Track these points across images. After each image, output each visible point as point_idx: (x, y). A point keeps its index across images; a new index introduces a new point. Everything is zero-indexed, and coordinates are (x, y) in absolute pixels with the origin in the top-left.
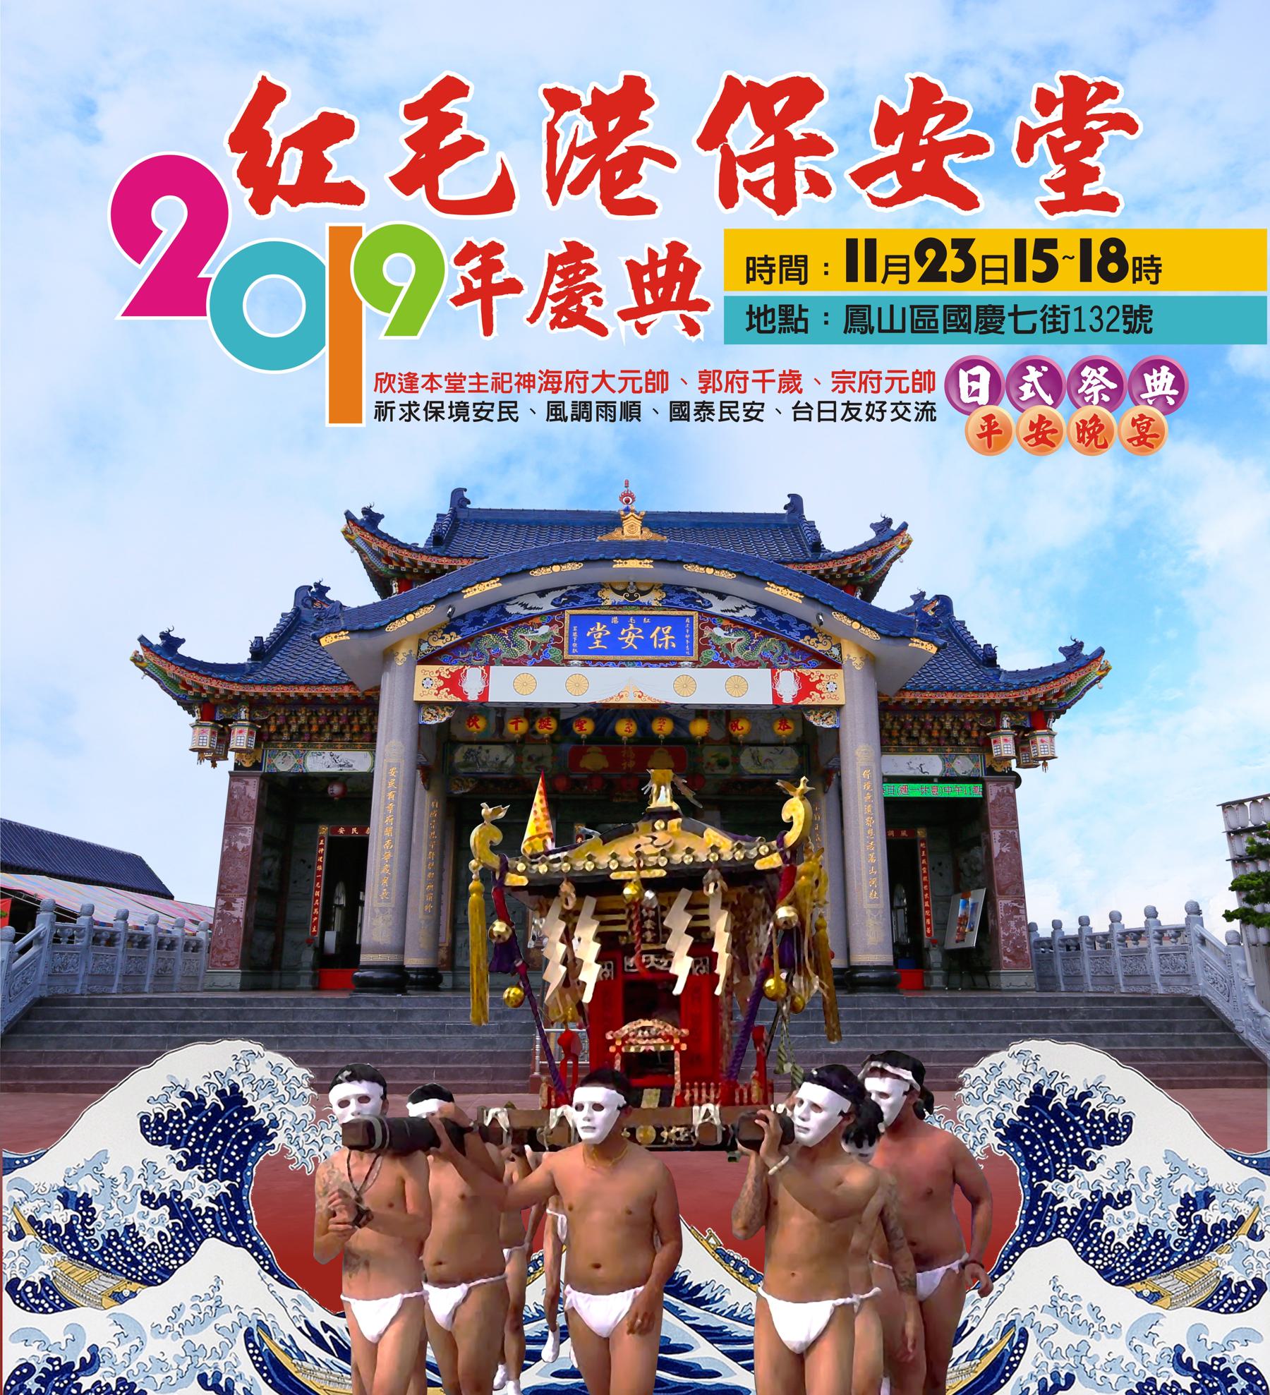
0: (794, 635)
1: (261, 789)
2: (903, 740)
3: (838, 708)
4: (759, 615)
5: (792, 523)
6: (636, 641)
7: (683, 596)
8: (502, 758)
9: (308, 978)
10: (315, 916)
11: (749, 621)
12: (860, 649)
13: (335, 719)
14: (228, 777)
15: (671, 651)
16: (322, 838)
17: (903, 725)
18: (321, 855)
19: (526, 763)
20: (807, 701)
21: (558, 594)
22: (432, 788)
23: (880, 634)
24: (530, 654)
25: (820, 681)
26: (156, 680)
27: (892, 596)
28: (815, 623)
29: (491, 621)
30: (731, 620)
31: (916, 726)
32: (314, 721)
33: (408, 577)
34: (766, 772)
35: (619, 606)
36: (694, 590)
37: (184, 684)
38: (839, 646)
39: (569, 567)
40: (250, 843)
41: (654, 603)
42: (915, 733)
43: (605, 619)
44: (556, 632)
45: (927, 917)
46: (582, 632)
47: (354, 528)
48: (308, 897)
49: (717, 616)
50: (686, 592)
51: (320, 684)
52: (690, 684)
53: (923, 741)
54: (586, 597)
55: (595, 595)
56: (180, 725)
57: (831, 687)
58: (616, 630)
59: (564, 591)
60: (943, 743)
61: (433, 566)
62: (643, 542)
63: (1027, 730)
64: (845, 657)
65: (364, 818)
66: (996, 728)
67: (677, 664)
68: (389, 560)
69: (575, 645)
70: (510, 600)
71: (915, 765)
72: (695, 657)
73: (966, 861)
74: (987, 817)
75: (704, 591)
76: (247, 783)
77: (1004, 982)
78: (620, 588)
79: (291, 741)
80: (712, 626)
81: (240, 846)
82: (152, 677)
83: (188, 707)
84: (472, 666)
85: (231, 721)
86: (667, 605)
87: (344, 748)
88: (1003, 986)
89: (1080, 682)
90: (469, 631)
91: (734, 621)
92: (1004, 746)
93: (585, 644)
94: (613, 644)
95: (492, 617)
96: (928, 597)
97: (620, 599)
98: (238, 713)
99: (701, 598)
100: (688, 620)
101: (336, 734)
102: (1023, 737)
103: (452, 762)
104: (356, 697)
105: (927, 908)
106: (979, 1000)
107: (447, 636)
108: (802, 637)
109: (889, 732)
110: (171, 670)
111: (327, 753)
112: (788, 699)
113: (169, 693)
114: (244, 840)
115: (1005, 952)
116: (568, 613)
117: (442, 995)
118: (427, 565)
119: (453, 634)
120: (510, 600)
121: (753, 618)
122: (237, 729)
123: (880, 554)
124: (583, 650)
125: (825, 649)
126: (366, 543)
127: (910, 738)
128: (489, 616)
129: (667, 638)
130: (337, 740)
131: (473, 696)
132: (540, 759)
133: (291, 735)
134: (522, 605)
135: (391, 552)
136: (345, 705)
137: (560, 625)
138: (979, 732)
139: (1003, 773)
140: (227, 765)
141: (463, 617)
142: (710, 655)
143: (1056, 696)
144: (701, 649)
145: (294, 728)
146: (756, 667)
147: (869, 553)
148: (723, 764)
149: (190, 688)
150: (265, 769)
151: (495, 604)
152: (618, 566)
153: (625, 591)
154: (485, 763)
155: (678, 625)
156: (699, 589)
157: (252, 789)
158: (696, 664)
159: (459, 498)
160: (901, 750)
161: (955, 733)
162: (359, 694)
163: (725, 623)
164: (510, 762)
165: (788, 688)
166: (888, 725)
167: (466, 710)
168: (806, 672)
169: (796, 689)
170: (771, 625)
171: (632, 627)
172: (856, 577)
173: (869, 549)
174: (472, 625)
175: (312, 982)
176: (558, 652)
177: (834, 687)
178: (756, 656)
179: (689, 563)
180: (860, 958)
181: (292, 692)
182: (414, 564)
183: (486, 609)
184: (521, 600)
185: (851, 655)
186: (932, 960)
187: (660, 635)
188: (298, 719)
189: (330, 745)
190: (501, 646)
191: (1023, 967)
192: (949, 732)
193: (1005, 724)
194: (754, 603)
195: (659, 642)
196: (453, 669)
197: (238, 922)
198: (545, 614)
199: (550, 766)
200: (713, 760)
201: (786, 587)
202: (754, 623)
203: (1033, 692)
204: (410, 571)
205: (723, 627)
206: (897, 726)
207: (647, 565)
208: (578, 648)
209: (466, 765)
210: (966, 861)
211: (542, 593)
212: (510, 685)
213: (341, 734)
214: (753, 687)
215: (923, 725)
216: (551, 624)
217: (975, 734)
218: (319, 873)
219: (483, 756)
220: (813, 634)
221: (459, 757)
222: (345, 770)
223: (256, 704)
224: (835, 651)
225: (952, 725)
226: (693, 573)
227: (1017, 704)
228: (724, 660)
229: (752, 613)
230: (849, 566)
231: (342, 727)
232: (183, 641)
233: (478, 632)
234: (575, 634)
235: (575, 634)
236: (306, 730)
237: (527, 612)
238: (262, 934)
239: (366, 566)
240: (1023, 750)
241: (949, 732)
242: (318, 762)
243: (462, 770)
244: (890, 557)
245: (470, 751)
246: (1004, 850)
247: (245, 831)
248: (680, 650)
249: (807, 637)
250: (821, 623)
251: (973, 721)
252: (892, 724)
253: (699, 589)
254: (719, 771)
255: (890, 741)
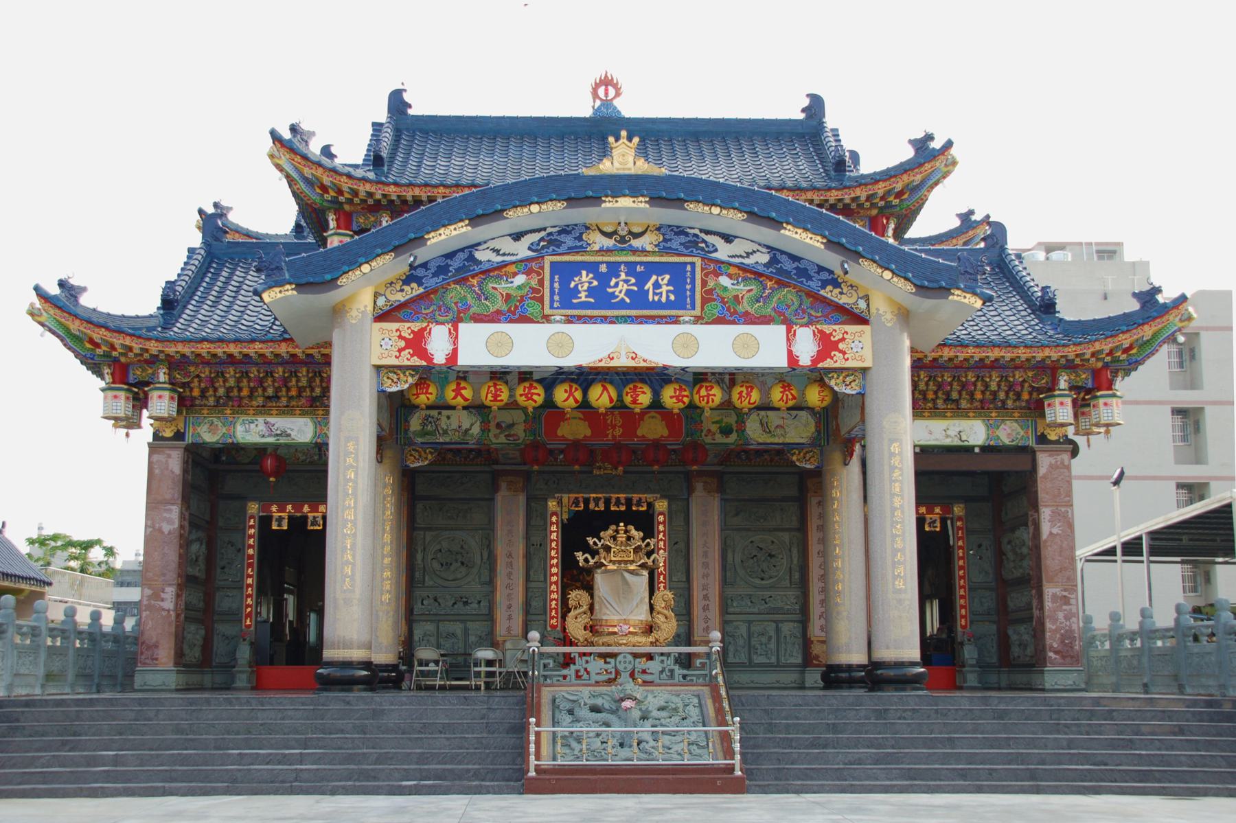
0: (814, 285)
1: (185, 462)
2: (940, 402)
3: (864, 371)
4: (773, 261)
5: (808, 132)
6: (628, 293)
7: (683, 239)
8: (466, 425)
9: (244, 677)
10: (248, 606)
11: (760, 269)
12: (891, 301)
13: (270, 380)
14: (147, 450)
15: (669, 305)
16: (252, 517)
17: (940, 386)
18: (251, 537)
19: (494, 431)
20: (828, 363)
21: (535, 237)
22: (385, 461)
23: (915, 285)
24: (505, 308)
25: (843, 339)
26: (58, 336)
27: (934, 218)
28: (838, 272)
29: (458, 270)
30: (741, 267)
31: (956, 386)
32: (244, 383)
33: (347, 207)
34: (776, 440)
35: (608, 251)
36: (697, 232)
37: (91, 341)
38: (867, 298)
39: (548, 207)
40: (176, 525)
41: (649, 248)
42: (955, 395)
43: (592, 267)
44: (534, 283)
45: (962, 607)
46: (565, 282)
47: (282, 150)
48: (239, 586)
49: (723, 262)
50: (687, 234)
51: (253, 341)
52: (691, 345)
53: (964, 404)
54: (569, 241)
55: (580, 238)
56: (88, 390)
57: (856, 346)
58: (604, 280)
59: (543, 234)
60: (986, 406)
61: (378, 197)
62: (638, 177)
63: (1089, 391)
64: (873, 310)
65: (318, 493)
66: (1051, 388)
67: (675, 320)
68: (324, 189)
69: (556, 298)
70: (479, 244)
71: (952, 432)
72: (698, 312)
73: (1009, 542)
74: (1036, 492)
75: (708, 232)
76: (169, 456)
77: (1050, 680)
78: (609, 229)
79: (219, 405)
80: (717, 275)
81: (166, 528)
82: (54, 333)
83: (96, 369)
84: (438, 323)
85: (148, 384)
86: (664, 249)
87: (281, 413)
88: (1047, 686)
89: (1155, 335)
90: (432, 282)
91: (743, 268)
92: (1061, 411)
93: (567, 298)
94: (601, 297)
95: (461, 266)
96: (977, 217)
97: (609, 243)
98: (155, 374)
99: (704, 241)
100: (689, 268)
101: (269, 398)
102: (1084, 399)
103: (406, 431)
104: (294, 356)
105: (962, 597)
106: (1020, 701)
107: (406, 288)
108: (823, 287)
109: (924, 393)
110: (75, 326)
111: (261, 420)
112: (805, 360)
113: (70, 348)
114: (169, 521)
115: (1051, 647)
116: (548, 260)
117: (404, 694)
118: (370, 195)
119: (414, 285)
120: (479, 244)
121: (767, 265)
122: (155, 394)
123: (918, 178)
124: (566, 303)
125: (851, 301)
126: (296, 168)
127: (948, 399)
128: (455, 263)
129: (664, 289)
130: (272, 404)
131: (440, 358)
132: (511, 426)
133: (218, 399)
134: (494, 250)
135: (326, 180)
136: (281, 364)
137: (539, 274)
138: (1030, 394)
139: (1057, 442)
140: (145, 433)
141: (424, 265)
142: (714, 309)
143: (1126, 351)
144: (705, 301)
145: (221, 392)
146: (768, 323)
147: (905, 177)
148: (726, 431)
149: (97, 345)
150: (189, 439)
151: (462, 250)
152: (608, 205)
153: (615, 232)
154: (445, 432)
155: (678, 274)
156: (701, 231)
157: (174, 462)
158: (698, 320)
159: (397, 103)
160: (936, 413)
161: (1002, 395)
162: (298, 351)
163: (732, 270)
164: (476, 430)
165: (806, 347)
166: (922, 386)
167: (426, 375)
168: (827, 329)
169: (815, 349)
170: (787, 273)
171: (623, 276)
172: (889, 206)
173: (906, 172)
174: (435, 275)
175: (249, 681)
176: (537, 306)
177: (858, 347)
178: (768, 311)
179: (691, 201)
180: (885, 654)
181: (219, 351)
182: (355, 193)
183: (451, 255)
184: (491, 244)
185: (880, 307)
186: (967, 656)
187: (657, 285)
188: (225, 381)
189: (263, 410)
190: (470, 299)
191: (1071, 665)
192: (995, 394)
193: (1063, 384)
194: (768, 247)
195: (654, 294)
196: (416, 326)
197: (169, 616)
198: (521, 261)
199: (521, 434)
200: (714, 428)
201: (806, 229)
202: (767, 271)
203: (1097, 346)
204: (350, 201)
205: (730, 276)
206: (932, 387)
207: (641, 204)
208: (560, 302)
209: (424, 433)
210: (1009, 542)
211: (517, 237)
212: (478, 346)
213: (276, 397)
214: (769, 347)
215: (964, 386)
216: (528, 272)
217: (1025, 396)
218: (251, 557)
219: (443, 423)
220: (836, 283)
221: (415, 424)
222: (283, 440)
223: (176, 364)
224: (862, 304)
225: (999, 386)
226: (697, 215)
227: (1078, 361)
228: (729, 315)
229: (764, 258)
230: (881, 193)
231: (277, 390)
232: (84, 289)
233: (445, 286)
234: (556, 285)
235: (556, 285)
236: (235, 393)
237: (500, 259)
238: (193, 628)
239: (294, 194)
240: (1083, 414)
241: (995, 394)
242: (251, 431)
243: (420, 440)
244: (931, 182)
245: (427, 418)
246: (1055, 531)
247: (170, 510)
248: (680, 304)
249: (829, 288)
250: (846, 273)
251: (1024, 381)
252: (927, 384)
253: (701, 231)
254: (720, 439)
255: (923, 405)
